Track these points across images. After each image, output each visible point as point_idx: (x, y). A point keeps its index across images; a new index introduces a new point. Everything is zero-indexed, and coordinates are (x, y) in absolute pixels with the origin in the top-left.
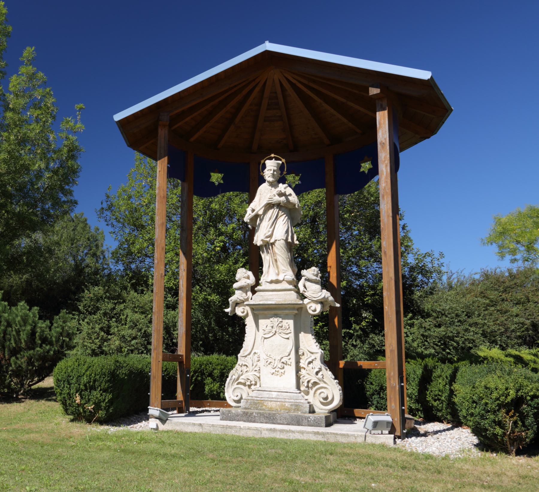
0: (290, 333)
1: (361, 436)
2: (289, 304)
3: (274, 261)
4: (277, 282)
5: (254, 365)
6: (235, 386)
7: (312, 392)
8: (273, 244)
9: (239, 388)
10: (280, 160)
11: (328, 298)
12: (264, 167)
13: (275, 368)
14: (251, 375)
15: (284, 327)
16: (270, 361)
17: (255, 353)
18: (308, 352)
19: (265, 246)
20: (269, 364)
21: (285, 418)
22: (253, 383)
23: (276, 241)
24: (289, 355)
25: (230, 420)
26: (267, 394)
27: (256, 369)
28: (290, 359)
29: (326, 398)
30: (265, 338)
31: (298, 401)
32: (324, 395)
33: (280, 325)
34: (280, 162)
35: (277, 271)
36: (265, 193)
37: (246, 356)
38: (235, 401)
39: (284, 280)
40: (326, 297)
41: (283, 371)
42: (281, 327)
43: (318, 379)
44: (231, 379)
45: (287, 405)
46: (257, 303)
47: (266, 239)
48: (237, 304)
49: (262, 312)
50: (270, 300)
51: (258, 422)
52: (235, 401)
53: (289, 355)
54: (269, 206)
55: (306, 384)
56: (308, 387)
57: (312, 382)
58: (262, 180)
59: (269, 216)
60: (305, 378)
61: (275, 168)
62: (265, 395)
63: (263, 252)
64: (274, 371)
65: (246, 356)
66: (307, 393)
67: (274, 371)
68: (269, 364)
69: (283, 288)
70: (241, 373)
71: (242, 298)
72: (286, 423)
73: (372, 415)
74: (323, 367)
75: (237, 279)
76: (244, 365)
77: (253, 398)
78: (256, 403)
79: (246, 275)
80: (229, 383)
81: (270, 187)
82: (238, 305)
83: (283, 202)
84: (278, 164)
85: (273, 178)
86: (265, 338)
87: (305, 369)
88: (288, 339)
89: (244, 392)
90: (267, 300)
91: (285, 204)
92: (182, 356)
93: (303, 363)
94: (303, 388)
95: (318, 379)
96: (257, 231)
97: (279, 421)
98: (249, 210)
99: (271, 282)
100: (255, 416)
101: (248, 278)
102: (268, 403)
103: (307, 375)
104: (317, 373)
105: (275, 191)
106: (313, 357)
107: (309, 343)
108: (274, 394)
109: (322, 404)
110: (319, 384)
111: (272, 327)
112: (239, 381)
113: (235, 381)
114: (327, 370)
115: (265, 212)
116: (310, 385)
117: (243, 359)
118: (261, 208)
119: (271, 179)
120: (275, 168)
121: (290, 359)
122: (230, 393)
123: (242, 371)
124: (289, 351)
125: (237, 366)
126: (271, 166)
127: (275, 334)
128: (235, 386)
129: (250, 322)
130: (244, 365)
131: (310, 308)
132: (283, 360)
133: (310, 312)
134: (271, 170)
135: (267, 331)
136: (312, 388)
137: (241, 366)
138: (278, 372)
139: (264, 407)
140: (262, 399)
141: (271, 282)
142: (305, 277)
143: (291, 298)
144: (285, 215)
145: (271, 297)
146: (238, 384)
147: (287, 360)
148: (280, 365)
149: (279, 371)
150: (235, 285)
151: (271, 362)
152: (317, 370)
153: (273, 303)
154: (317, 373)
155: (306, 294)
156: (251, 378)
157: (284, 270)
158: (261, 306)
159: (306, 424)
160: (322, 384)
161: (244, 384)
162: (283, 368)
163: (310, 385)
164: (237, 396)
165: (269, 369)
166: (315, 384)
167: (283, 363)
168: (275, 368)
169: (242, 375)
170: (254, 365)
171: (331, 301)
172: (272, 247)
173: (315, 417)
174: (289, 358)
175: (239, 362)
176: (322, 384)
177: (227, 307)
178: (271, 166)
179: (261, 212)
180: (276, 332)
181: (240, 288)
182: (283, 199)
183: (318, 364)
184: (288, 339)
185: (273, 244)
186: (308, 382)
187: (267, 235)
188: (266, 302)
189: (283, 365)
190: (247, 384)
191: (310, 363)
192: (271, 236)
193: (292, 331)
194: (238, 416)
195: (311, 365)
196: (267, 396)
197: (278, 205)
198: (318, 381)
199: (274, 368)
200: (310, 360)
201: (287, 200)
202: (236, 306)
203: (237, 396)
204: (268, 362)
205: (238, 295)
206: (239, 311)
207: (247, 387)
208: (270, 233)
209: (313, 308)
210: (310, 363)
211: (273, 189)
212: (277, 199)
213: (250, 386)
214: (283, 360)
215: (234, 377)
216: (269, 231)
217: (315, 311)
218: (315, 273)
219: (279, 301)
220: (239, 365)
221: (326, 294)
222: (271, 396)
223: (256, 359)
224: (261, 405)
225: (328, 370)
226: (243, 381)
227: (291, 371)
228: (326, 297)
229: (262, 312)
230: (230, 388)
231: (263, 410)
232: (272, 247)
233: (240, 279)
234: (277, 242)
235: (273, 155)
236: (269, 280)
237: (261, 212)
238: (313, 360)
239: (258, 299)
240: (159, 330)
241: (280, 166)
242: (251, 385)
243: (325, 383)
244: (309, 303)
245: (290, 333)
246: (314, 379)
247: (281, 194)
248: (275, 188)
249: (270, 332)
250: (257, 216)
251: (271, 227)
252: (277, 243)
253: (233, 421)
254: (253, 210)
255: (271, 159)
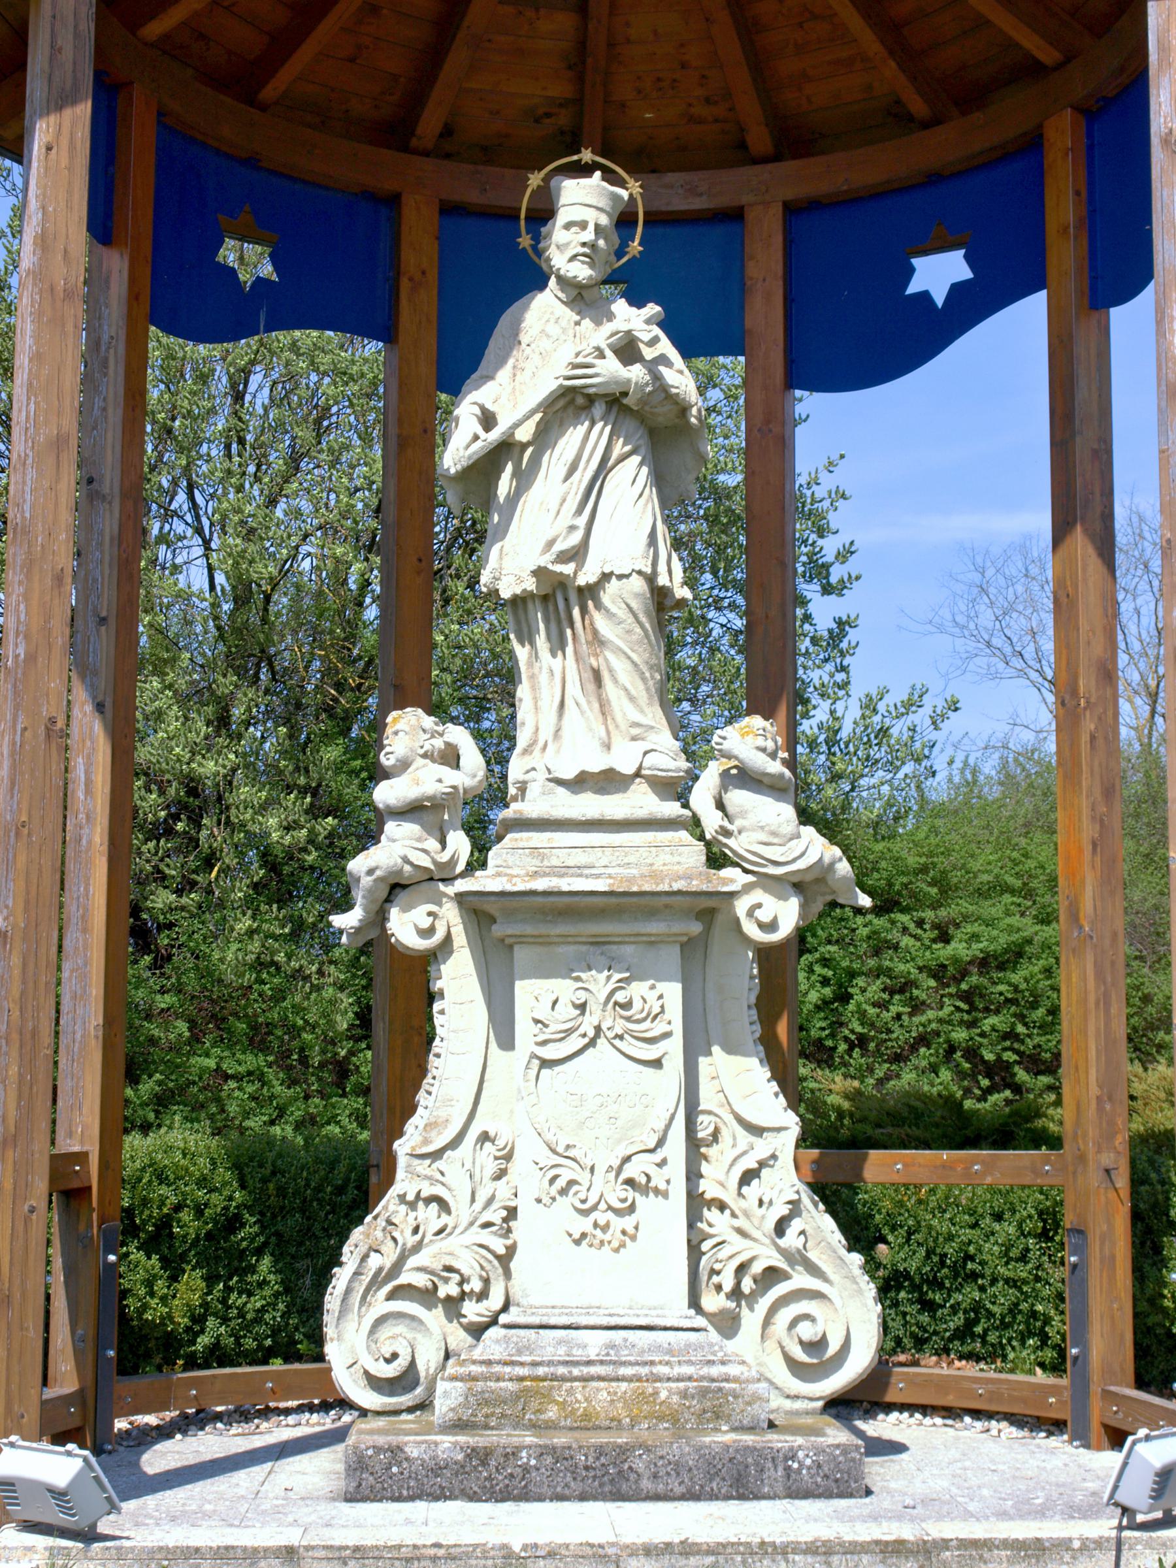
0: (667, 1035)
1: (1099, 1543)
2: (679, 893)
3: (588, 675)
4: (609, 781)
5: (481, 1199)
6: (380, 1305)
7: (751, 1320)
8: (590, 593)
9: (400, 1315)
10: (622, 184)
11: (832, 865)
12: (543, 214)
13: (595, 1208)
14: (463, 1251)
15: (637, 1005)
16: (566, 1175)
17: (485, 1137)
18: (740, 1131)
19: (545, 598)
20: (563, 1192)
21: (678, 1467)
22: (476, 1285)
23: (606, 577)
24: (661, 1143)
25: (399, 1499)
26: (560, 1342)
27: (486, 1217)
28: (662, 1163)
29: (816, 1346)
30: (546, 1063)
31: (715, 1371)
32: (806, 1331)
33: (620, 997)
34: (625, 194)
35: (603, 734)
36: (550, 342)
37: (437, 1155)
38: (375, 1383)
39: (638, 774)
40: (827, 860)
41: (628, 1222)
42: (627, 1006)
43: (783, 1252)
44: (357, 1273)
45: (663, 1395)
46: (521, 886)
47: (558, 568)
48: (396, 888)
49: (515, 932)
50: (579, 870)
51: (540, 1499)
52: (375, 1383)
53: (661, 1143)
54: (570, 404)
55: (727, 1280)
56: (736, 1293)
57: (757, 1268)
58: (534, 277)
59: (570, 456)
60: (724, 1253)
61: (604, 220)
62: (549, 1345)
63: (527, 637)
64: (586, 1224)
65: (437, 1155)
66: (728, 1324)
67: (586, 1224)
68: (563, 1192)
69: (641, 814)
70: (411, 1240)
71: (426, 862)
72: (679, 1490)
73: (1147, 1438)
74: (807, 1199)
75: (386, 761)
76: (429, 1200)
77: (497, 1369)
78: (529, 1395)
79: (439, 743)
80: (348, 1291)
81: (570, 315)
82: (403, 896)
83: (640, 387)
84: (615, 198)
85: (592, 265)
86: (546, 1063)
87: (722, 1207)
88: (657, 1064)
89: (428, 1338)
90: (563, 871)
91: (645, 400)
92: (81, 1157)
93: (717, 1179)
94: (712, 1302)
95: (783, 1252)
96: (502, 531)
97: (646, 1484)
98: (466, 411)
99: (580, 782)
100: (526, 1469)
101: (450, 757)
102: (570, 1392)
103: (740, 1241)
104: (780, 1228)
105: (599, 335)
106: (763, 1148)
107: (743, 1084)
108: (593, 1343)
109: (793, 1365)
110: (787, 1277)
111: (582, 1007)
112: (403, 1279)
113: (378, 1280)
114: (816, 1205)
115: (545, 436)
116: (747, 1285)
117: (422, 1167)
118: (527, 417)
119: (582, 272)
120: (604, 220)
121: (662, 1163)
122: (354, 1344)
123: (416, 1230)
124: (661, 1126)
125: (389, 1204)
126: (584, 203)
127: (592, 1043)
128: (380, 1305)
129: (459, 983)
130: (429, 1200)
131: (750, 913)
132: (629, 1171)
133: (751, 929)
134: (583, 225)
135: (553, 1027)
136: (752, 1299)
137: (412, 1206)
138: (605, 1228)
139: (552, 1413)
140: (541, 1371)
141: (580, 782)
142: (726, 764)
143: (674, 862)
144: (636, 459)
145: (580, 858)
146: (390, 1297)
147: (653, 1171)
148: (616, 1194)
149: (604, 1225)
150: (385, 794)
151: (572, 1183)
152: (785, 1210)
153: (601, 886)
154: (780, 1228)
155: (734, 844)
156: (467, 1263)
157: (636, 725)
158: (540, 899)
159: (779, 1488)
160: (801, 1280)
161: (427, 1296)
162: (632, 1209)
163: (747, 1285)
164: (395, 1356)
165: (564, 1213)
166: (772, 1275)
167: (630, 1182)
168: (595, 1208)
169: (417, 1248)
170: (481, 1199)
171: (844, 878)
172: (584, 611)
173: (819, 1451)
174: (657, 1157)
175: (404, 1184)
176: (801, 1280)
177: (344, 905)
178: (584, 203)
179: (524, 434)
180: (598, 1029)
181: (412, 811)
182: (636, 373)
183: (784, 1183)
184: (657, 1064)
185: (590, 593)
186: (742, 1269)
187: (560, 546)
188: (565, 884)
189: (631, 1194)
190: (442, 1293)
191: (748, 1177)
192: (578, 554)
193: (678, 1028)
194: (437, 1469)
195: (753, 1190)
196: (561, 1353)
197: (616, 404)
198: (782, 1264)
199: (585, 1213)
200: (750, 1163)
201: (657, 377)
202: (388, 900)
203: (395, 1356)
204: (561, 1183)
205: (398, 847)
206: (405, 927)
207: (439, 1311)
208: (576, 538)
209: (764, 915)
210: (748, 1177)
211: (587, 323)
212: (610, 368)
213: (452, 1306)
214: (629, 1171)
215: (375, 1261)
216: (572, 528)
217: (771, 926)
218: (770, 745)
219: (631, 880)
220: (402, 1198)
221: (814, 847)
222: (578, 1354)
223: (492, 1167)
224: (534, 1405)
225: (821, 1206)
226: (421, 1280)
227: (665, 1219)
228: (827, 860)
229: (515, 932)
230: (353, 1316)
231: (551, 1426)
232: (584, 611)
233: (404, 765)
234: (613, 586)
235: (587, 156)
236: (569, 774)
237: (524, 434)
238: (762, 1164)
239: (511, 868)
240: (35, 1033)
241: (620, 209)
242: (463, 1296)
243: (814, 1270)
244: (748, 888)
245: (667, 1035)
246: (768, 1257)
247: (627, 350)
248: (598, 323)
249: (569, 1032)
250: (505, 449)
251: (579, 511)
252: (610, 594)
253: (411, 1499)
254: (488, 420)
255: (584, 170)
